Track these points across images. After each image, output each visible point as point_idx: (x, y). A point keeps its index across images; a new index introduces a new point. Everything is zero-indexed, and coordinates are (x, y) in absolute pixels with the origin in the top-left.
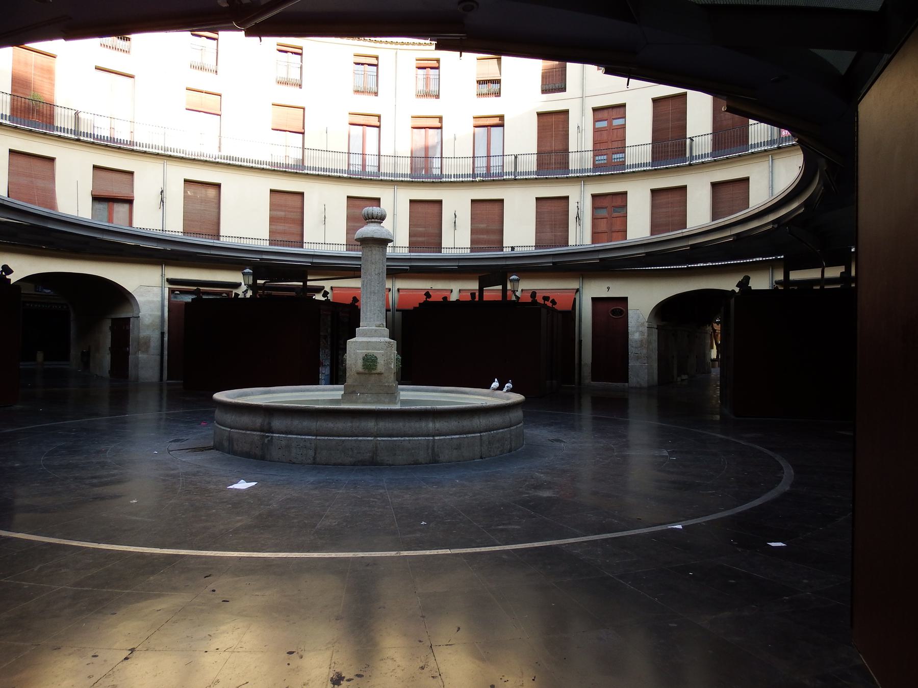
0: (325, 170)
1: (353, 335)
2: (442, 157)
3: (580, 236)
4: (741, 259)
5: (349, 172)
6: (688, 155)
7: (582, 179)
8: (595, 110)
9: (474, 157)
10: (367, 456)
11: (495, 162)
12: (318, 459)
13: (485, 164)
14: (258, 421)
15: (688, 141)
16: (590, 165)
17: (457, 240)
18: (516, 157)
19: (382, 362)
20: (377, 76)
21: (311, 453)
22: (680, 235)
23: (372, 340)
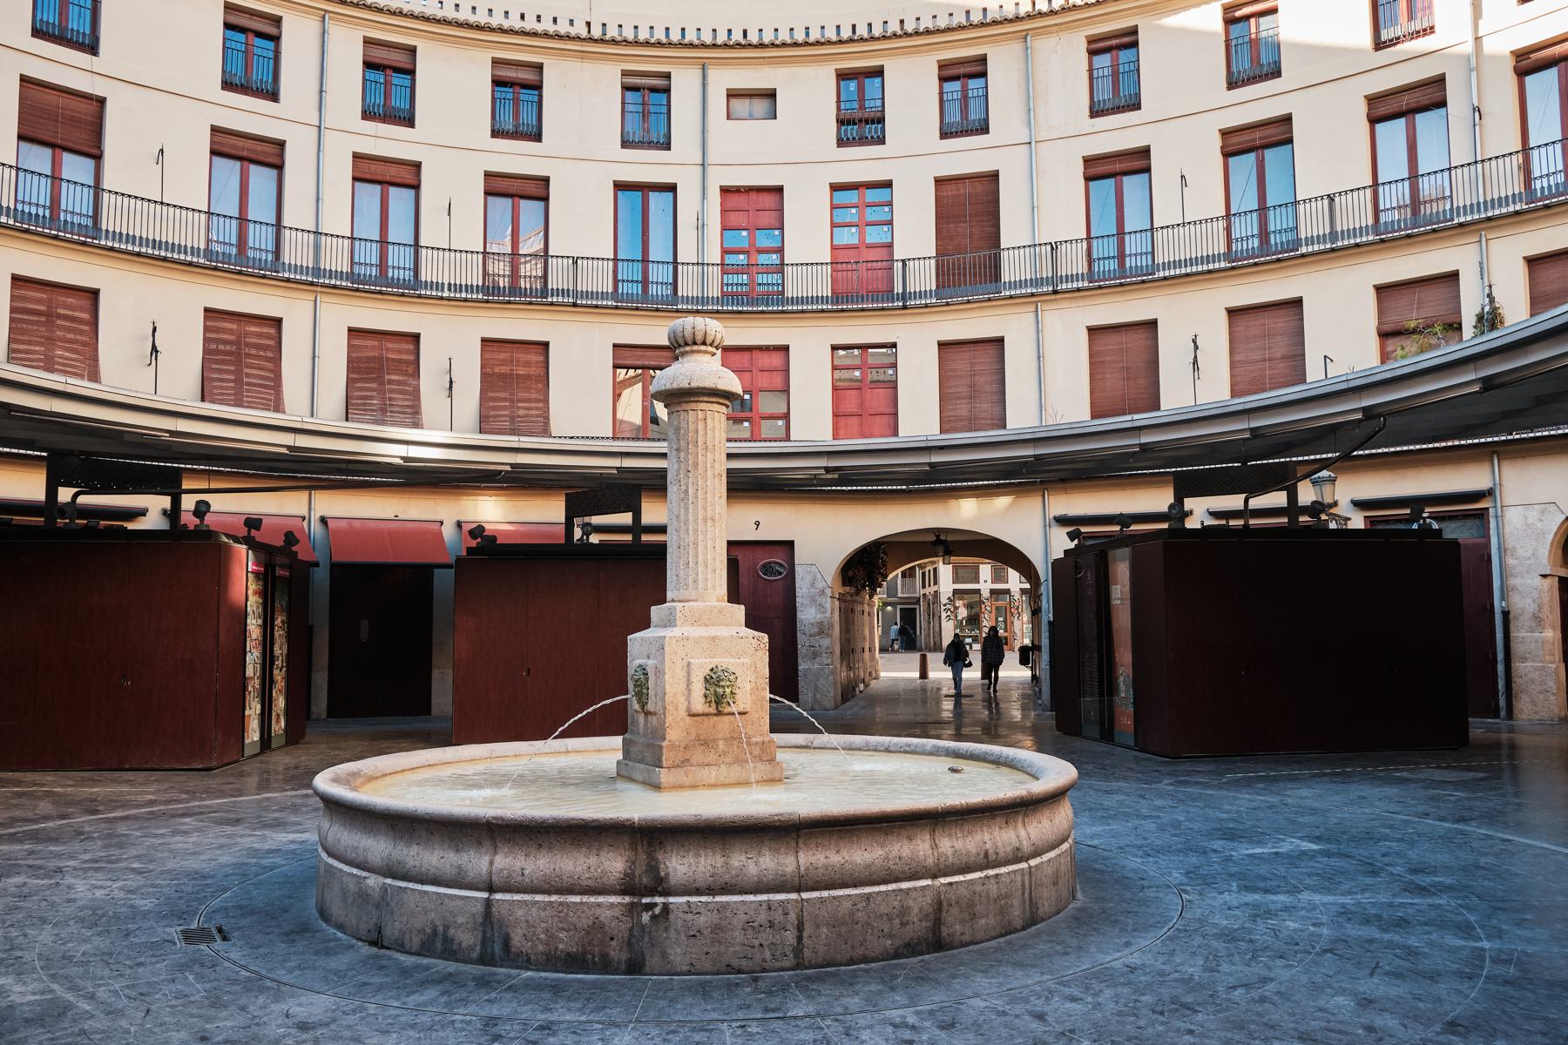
0: (155, 244)
1: (645, 624)
2: (417, 245)
3: (919, 417)
4: (1453, 439)
5: (208, 253)
6: (898, 289)
7: (806, 309)
8: (725, 190)
9: (1089, 238)
10: (918, 927)
11: (1133, 245)
12: (807, 953)
13: (1113, 252)
14: (613, 864)
15: (898, 266)
16: (714, 291)
17: (1197, 377)
18: (575, 262)
19: (748, 686)
20: (1091, 78)
21: (790, 937)
22: (1240, 408)
23: (696, 640)
